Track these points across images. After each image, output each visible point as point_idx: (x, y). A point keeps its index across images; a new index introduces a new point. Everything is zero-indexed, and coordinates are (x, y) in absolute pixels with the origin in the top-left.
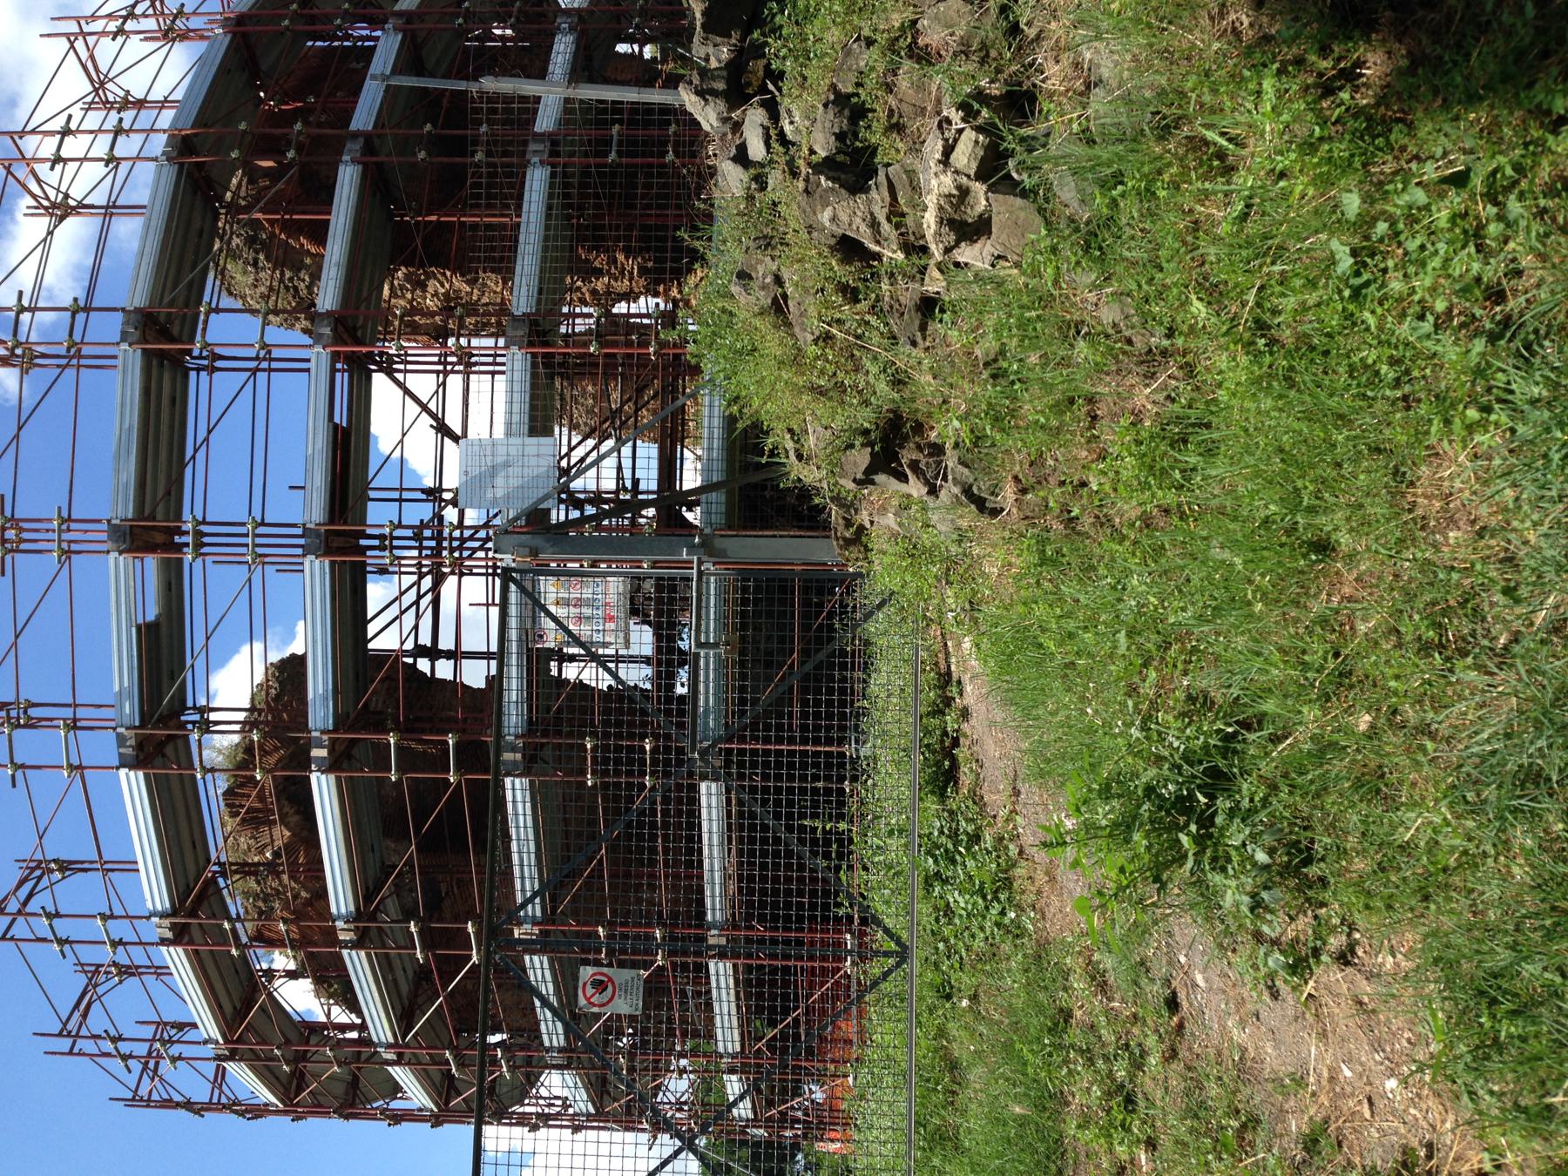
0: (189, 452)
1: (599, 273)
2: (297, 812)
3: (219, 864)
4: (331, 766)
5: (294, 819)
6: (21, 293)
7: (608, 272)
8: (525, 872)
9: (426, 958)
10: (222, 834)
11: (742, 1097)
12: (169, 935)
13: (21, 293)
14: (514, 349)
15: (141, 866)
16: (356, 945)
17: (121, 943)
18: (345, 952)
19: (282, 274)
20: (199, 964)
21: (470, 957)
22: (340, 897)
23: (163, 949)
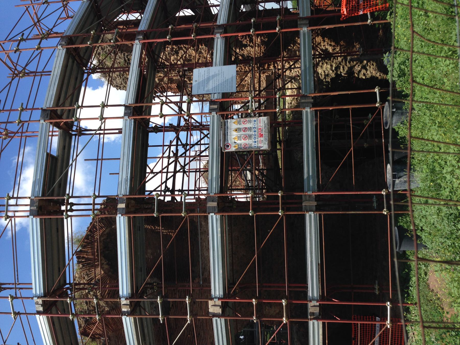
0: (67, 262)
1: (246, 46)
2: (108, 264)
3: (70, 284)
4: (127, 212)
5: (106, 267)
6: (22, 104)
7: (249, 45)
8: (217, 287)
9: (164, 320)
10: (73, 271)
11: (288, 89)
12: (41, 309)
13: (22, 104)
14: (214, 113)
15: (33, 286)
16: (129, 314)
17: (19, 313)
18: (123, 318)
19: (124, 55)
20: (52, 324)
21: (186, 320)
22: (124, 287)
23: (37, 316)
